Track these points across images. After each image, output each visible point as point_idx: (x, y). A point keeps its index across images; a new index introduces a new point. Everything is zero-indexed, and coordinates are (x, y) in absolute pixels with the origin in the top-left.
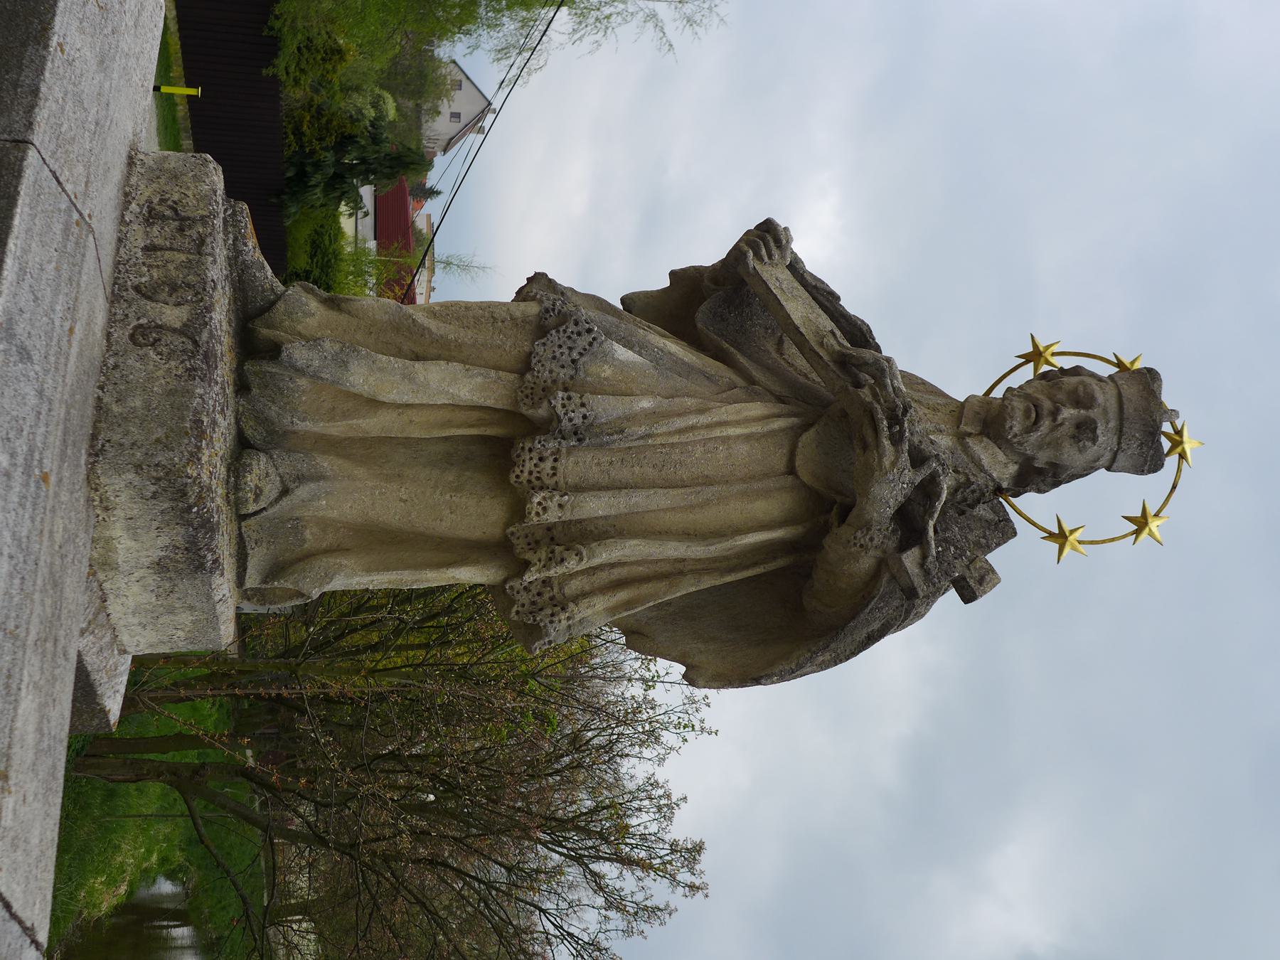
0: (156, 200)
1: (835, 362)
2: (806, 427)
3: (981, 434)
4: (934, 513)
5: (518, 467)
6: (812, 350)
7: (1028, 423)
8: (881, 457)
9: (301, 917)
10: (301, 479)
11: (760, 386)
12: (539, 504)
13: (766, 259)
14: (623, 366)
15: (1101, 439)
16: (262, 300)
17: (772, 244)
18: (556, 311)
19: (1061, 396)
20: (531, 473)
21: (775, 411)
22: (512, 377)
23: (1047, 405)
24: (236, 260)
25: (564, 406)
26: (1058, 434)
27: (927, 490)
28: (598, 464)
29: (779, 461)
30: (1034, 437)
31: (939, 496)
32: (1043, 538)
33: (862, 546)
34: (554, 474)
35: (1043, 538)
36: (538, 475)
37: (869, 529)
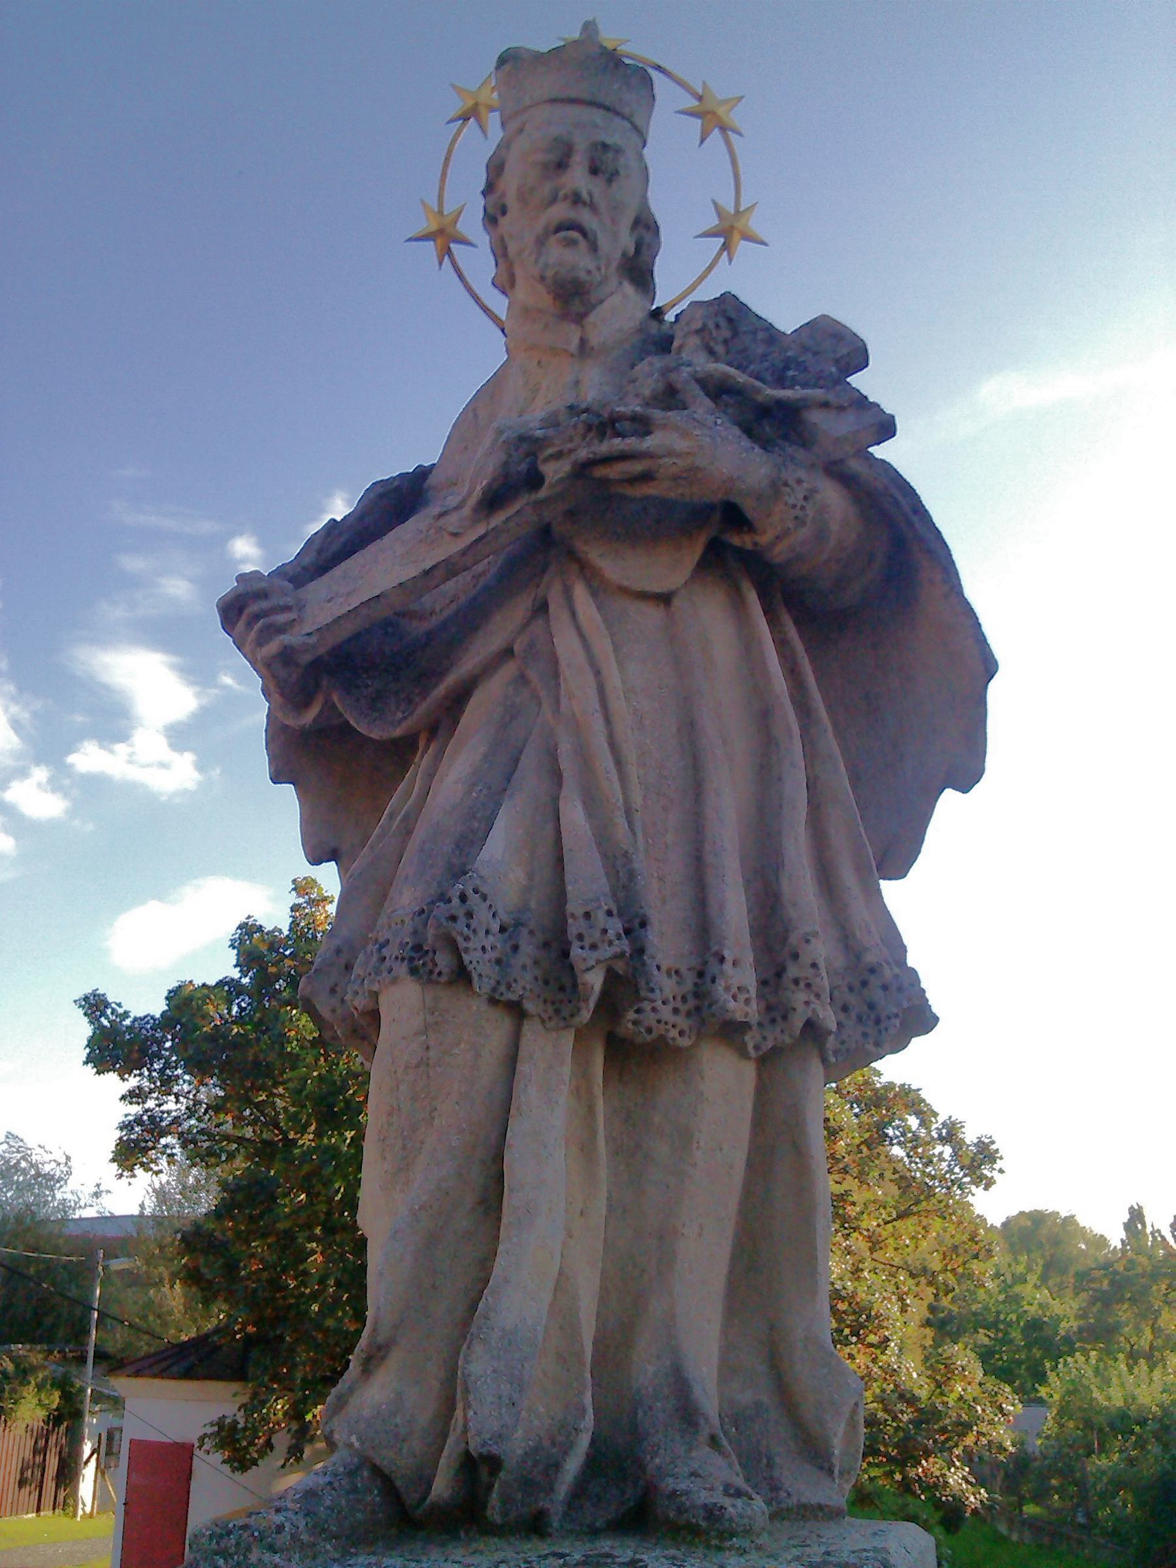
1: (488, 516)
2: (587, 571)
4: (753, 387)
5: (667, 1030)
6: (464, 553)
7: (583, 244)
8: (671, 453)
9: (974, 1481)
11: (514, 640)
12: (734, 997)
13: (292, 616)
16: (371, 1492)
18: (414, 955)
19: (546, 189)
21: (565, 616)
23: (560, 212)
25: (594, 947)
27: (718, 390)
30: (603, 241)
31: (727, 376)
32: (730, 260)
33: (806, 498)
34: (677, 972)
35: (730, 260)
36: (679, 998)
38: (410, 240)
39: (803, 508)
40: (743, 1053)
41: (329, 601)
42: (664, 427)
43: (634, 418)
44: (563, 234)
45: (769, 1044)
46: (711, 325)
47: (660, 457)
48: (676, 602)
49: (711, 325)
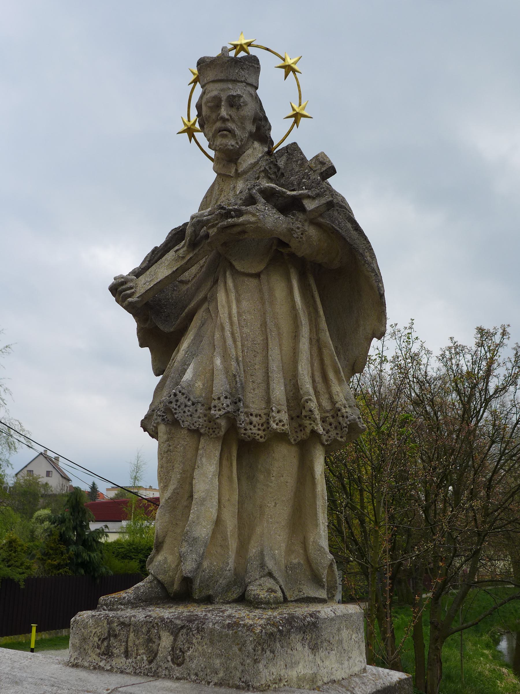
0: (98, 651)
3: (236, 164)
4: (283, 191)
6: (186, 263)
7: (230, 135)
8: (250, 223)
10: (263, 565)
11: (207, 294)
12: (277, 424)
13: (133, 290)
14: (196, 375)
15: (239, 92)
17: (124, 287)
20: (259, 429)
22: (202, 441)
24: (133, 604)
25: (220, 410)
26: (236, 118)
28: (254, 389)
29: (252, 283)
30: (238, 132)
31: (273, 188)
33: (302, 234)
34: (260, 415)
36: (260, 425)
37: (292, 230)
38: (179, 133)
39: (301, 238)
40: (290, 443)
41: (145, 284)
42: (246, 213)
43: (235, 210)
44: (221, 133)
45: (299, 439)
46: (267, 168)
47: (246, 225)
48: (262, 276)
49: (267, 168)
